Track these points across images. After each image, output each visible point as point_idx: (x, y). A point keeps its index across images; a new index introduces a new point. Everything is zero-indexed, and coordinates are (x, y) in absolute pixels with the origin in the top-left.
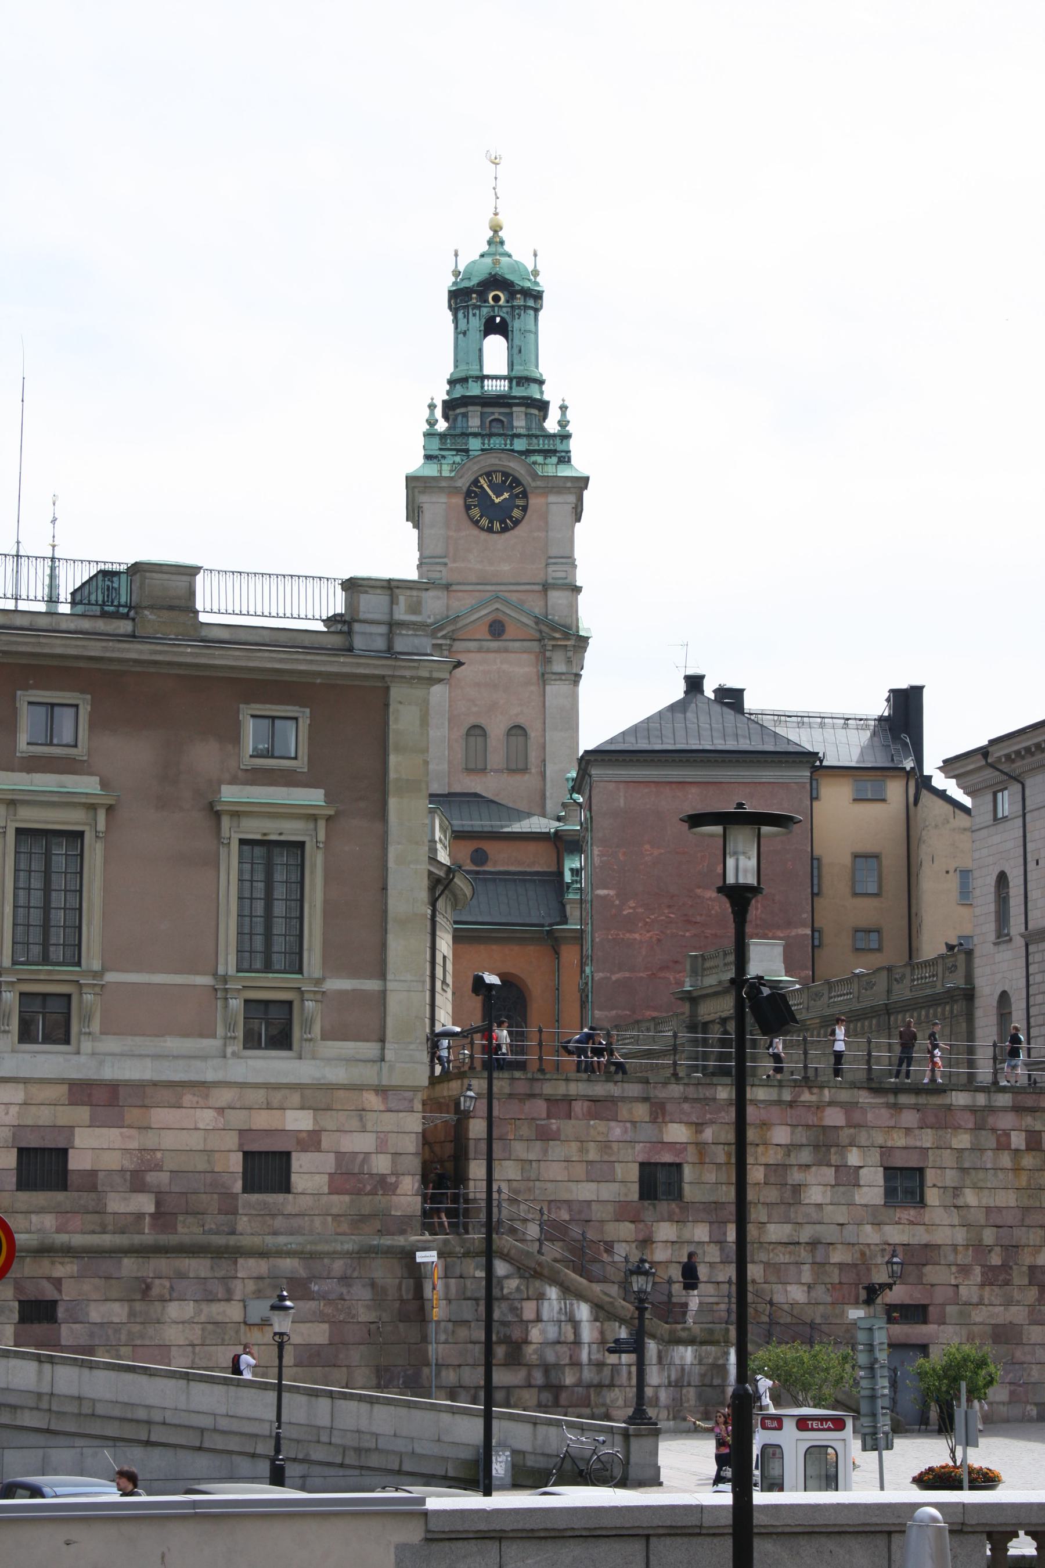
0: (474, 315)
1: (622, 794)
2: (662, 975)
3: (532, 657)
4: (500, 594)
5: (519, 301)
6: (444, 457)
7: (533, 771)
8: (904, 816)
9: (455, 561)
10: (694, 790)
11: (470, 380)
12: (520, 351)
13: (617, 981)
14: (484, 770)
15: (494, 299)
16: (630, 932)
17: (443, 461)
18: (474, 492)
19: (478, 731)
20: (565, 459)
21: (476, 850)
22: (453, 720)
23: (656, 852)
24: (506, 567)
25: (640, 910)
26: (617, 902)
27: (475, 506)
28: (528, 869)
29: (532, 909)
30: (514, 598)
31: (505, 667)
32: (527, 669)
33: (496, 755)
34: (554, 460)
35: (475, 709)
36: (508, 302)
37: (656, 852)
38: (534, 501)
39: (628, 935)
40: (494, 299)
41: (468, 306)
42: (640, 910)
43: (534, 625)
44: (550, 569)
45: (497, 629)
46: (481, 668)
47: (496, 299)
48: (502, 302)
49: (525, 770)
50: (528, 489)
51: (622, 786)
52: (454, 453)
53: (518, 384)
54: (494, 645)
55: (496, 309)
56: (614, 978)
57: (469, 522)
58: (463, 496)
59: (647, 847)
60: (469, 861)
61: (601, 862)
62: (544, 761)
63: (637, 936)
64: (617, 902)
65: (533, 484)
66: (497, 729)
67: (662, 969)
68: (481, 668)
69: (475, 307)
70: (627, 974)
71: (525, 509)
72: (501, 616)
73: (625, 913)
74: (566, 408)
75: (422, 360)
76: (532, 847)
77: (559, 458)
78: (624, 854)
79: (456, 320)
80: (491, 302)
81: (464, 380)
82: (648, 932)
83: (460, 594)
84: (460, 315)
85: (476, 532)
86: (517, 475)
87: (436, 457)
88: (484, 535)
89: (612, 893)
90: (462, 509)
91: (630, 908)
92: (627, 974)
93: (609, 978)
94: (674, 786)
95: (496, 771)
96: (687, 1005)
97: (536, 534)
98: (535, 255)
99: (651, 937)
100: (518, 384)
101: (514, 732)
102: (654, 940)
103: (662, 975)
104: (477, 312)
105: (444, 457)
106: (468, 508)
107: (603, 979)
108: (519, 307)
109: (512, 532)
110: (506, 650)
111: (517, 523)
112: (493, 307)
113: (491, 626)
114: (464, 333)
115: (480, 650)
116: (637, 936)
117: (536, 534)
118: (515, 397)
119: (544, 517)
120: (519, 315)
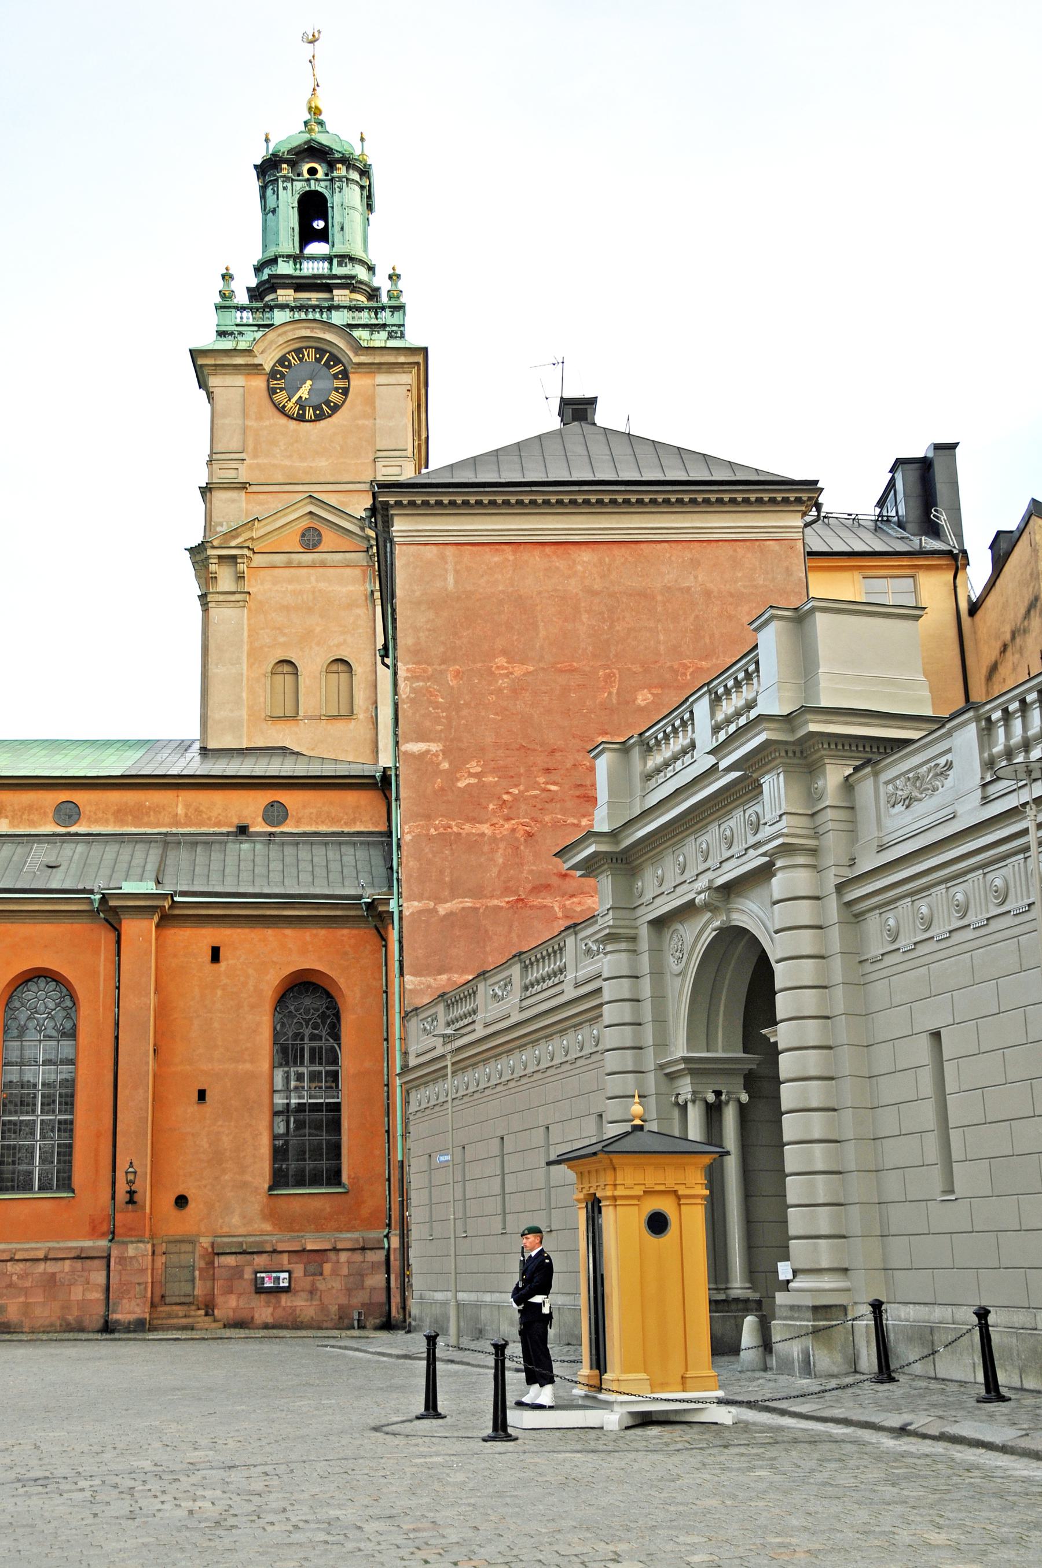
0: (285, 188)
1: (450, 567)
2: (537, 901)
3: (358, 572)
4: (315, 495)
5: (341, 170)
6: (241, 333)
7: (361, 716)
8: (953, 633)
9: (255, 456)
10: (586, 556)
11: (280, 260)
12: (342, 229)
13: (450, 914)
14: (294, 717)
15: (311, 180)
16: (473, 820)
17: (240, 338)
18: (281, 372)
19: (286, 668)
20: (397, 331)
21: (272, 804)
22: (255, 654)
23: (519, 670)
24: (322, 463)
25: (490, 779)
26: (445, 765)
27: (281, 389)
28: (346, 830)
29: (347, 877)
30: (332, 500)
31: (322, 585)
32: (351, 588)
33: (314, 686)
34: (384, 335)
35: (282, 639)
36: (327, 175)
37: (519, 670)
38: (357, 382)
39: (467, 827)
40: (311, 180)
41: (277, 180)
42: (490, 779)
43: (357, 531)
44: (379, 465)
45: (311, 540)
46: (290, 587)
47: (312, 171)
48: (320, 175)
49: (350, 715)
50: (350, 369)
51: (450, 551)
52: (256, 328)
53: (340, 264)
54: (308, 558)
55: (312, 182)
56: (442, 910)
57: (274, 410)
58: (265, 378)
59: (501, 661)
60: (260, 819)
61: (413, 690)
62: (376, 702)
63: (485, 828)
64: (445, 765)
65: (356, 360)
66: (312, 664)
67: (538, 889)
68: (290, 587)
69: (286, 179)
70: (468, 903)
71: (345, 392)
72: (316, 524)
73: (461, 784)
74: (398, 276)
75: (237, 232)
76: (351, 797)
77: (389, 333)
78: (457, 674)
79: (263, 197)
80: (306, 176)
81: (273, 261)
82: (508, 819)
83: (261, 496)
84: (269, 192)
85: (284, 420)
86: (335, 351)
87: (232, 333)
88: (293, 424)
89: (434, 747)
90: (265, 394)
91: (471, 775)
92: (468, 903)
93: (434, 911)
94: (548, 550)
95: (311, 718)
96: (605, 883)
97: (360, 422)
98: (362, 139)
99: (513, 830)
100: (340, 264)
101: (334, 668)
102: (520, 834)
103: (537, 901)
104: (289, 185)
105: (241, 333)
106: (272, 391)
107: (420, 912)
108: (340, 179)
109: (329, 419)
110: (323, 565)
111: (335, 408)
112: (308, 180)
113: (303, 535)
114: (274, 211)
115: (288, 566)
116: (485, 828)
117: (360, 422)
118: (336, 277)
119: (370, 401)
120: (341, 189)
